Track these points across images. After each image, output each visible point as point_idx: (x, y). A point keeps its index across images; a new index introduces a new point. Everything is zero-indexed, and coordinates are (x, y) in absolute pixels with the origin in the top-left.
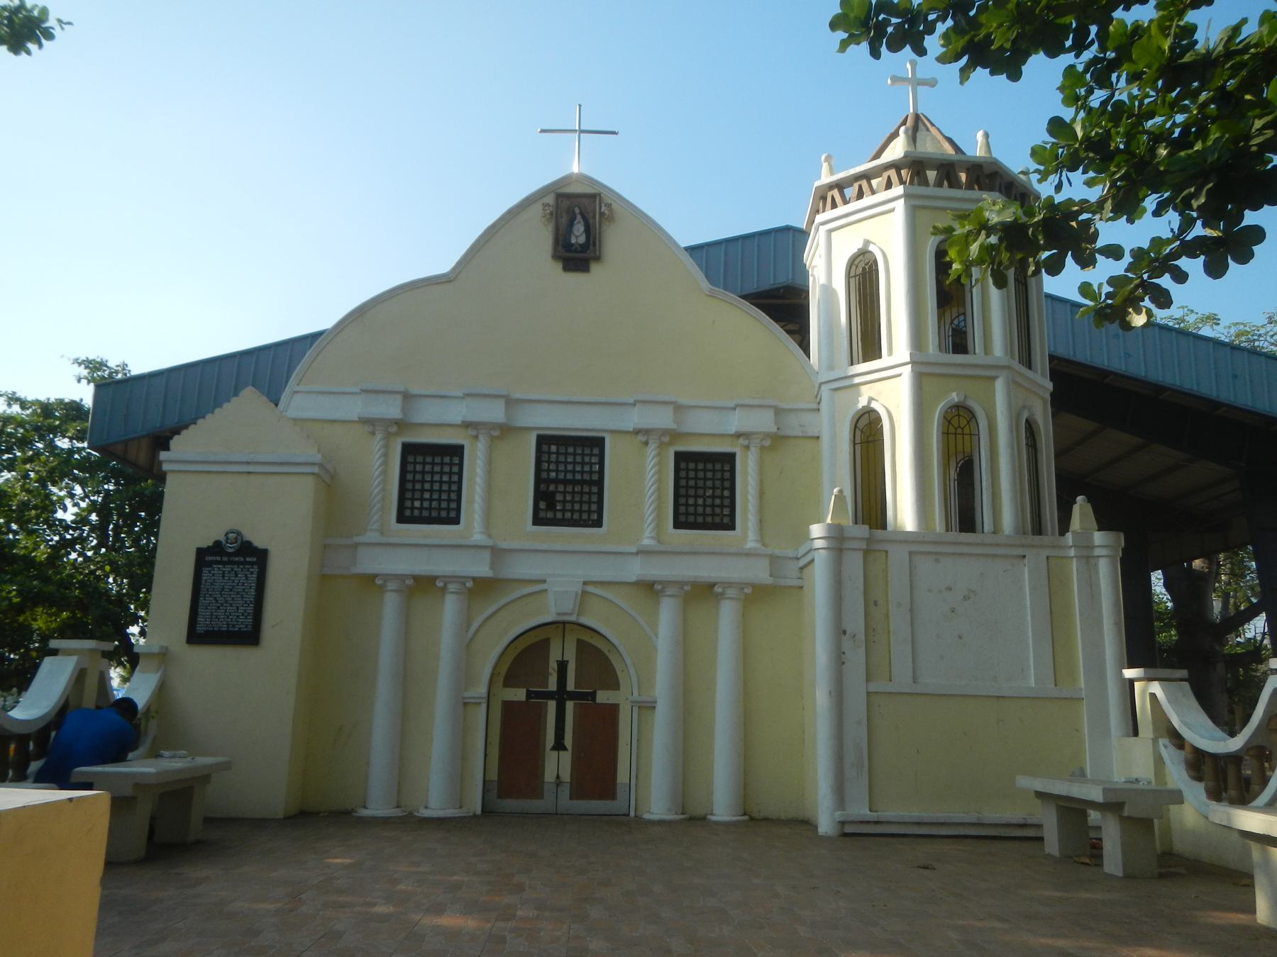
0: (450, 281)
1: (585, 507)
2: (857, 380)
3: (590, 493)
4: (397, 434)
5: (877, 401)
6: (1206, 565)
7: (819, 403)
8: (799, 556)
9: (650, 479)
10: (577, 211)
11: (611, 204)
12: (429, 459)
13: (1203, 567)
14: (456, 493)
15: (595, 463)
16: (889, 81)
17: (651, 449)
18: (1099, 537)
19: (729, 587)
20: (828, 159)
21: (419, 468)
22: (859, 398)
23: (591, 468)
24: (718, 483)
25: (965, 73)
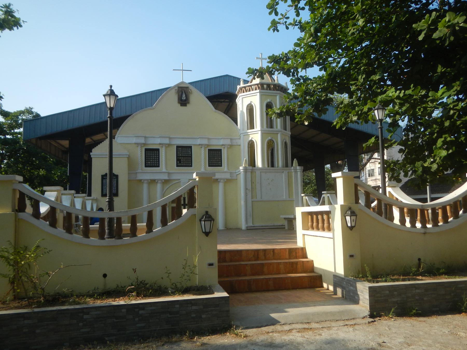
1: (188, 162)
2: (249, 133)
4: (143, 146)
10: (183, 91)
12: (151, 152)
18: (298, 167)
21: (149, 154)
24: (218, 156)
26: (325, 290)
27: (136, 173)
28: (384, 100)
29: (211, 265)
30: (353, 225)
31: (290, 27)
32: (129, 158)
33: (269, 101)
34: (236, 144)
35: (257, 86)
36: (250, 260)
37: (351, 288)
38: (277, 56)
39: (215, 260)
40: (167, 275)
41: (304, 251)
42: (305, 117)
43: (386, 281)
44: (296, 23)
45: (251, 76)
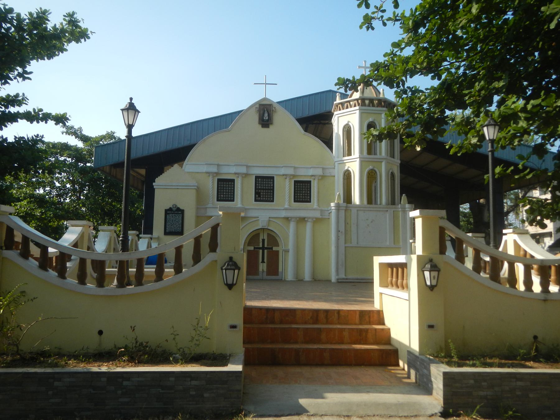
2: (345, 161)
12: (225, 183)
21: (222, 186)
24: (306, 189)
26: (400, 370)
27: (206, 208)
28: (504, 114)
29: (233, 327)
30: (434, 283)
31: (389, 23)
32: (198, 190)
35: (356, 102)
36: (306, 323)
37: (425, 371)
38: (381, 63)
39: (239, 321)
40: (173, 336)
41: (381, 315)
42: (417, 140)
43: (474, 365)
44: (397, 18)
45: (342, 88)
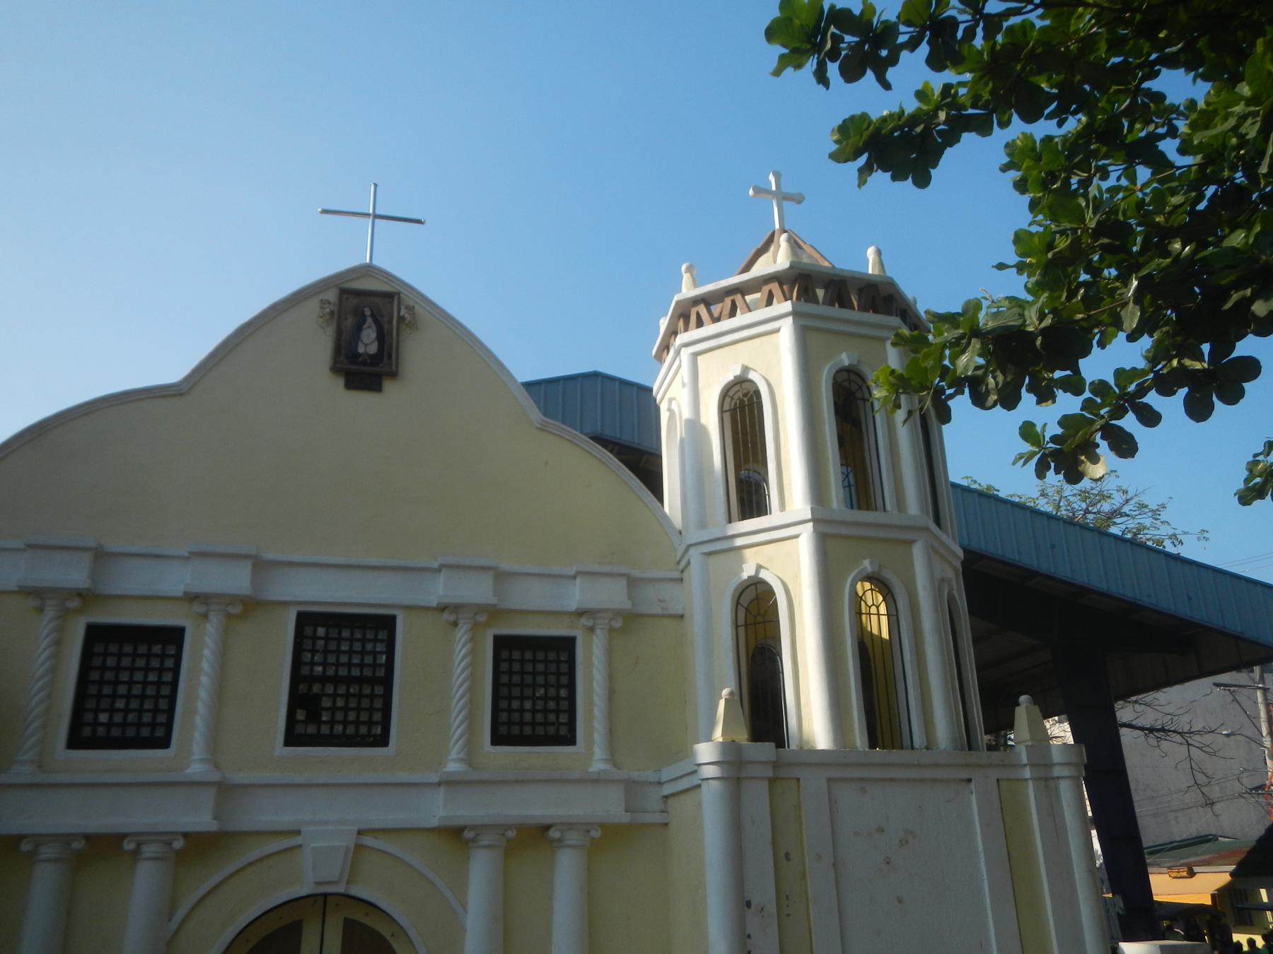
0: (181, 395)
1: (364, 717)
2: (739, 542)
3: (372, 697)
4: (79, 611)
5: (768, 569)
6: (993, 738)
7: (682, 571)
8: (662, 781)
9: (461, 674)
10: (368, 312)
11: (413, 307)
13: (990, 740)
14: (167, 700)
15: (381, 653)
16: (751, 192)
17: (462, 631)
19: (570, 829)
20: (689, 270)
22: (743, 566)
23: (375, 659)
24: (552, 679)
25: (865, 171)
33: (847, 363)
34: (659, 611)
